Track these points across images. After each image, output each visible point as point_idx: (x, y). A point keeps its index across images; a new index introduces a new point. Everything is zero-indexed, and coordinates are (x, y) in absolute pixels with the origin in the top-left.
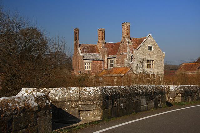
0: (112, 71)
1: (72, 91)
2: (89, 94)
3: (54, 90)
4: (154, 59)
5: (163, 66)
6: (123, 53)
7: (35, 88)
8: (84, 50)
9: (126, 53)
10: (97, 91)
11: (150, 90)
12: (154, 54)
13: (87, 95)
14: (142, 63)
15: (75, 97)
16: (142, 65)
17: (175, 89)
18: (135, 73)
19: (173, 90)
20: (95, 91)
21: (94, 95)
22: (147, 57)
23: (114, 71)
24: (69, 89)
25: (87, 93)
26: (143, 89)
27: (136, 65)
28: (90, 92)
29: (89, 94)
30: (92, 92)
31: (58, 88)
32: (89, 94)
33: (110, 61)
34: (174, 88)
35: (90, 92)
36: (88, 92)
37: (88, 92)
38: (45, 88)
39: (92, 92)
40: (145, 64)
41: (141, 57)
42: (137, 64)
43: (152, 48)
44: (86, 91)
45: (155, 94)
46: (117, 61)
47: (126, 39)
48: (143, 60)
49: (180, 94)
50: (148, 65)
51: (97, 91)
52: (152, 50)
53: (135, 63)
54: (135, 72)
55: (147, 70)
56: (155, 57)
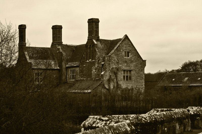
0: (74, 85)
1: (132, 118)
2: (146, 121)
3: (117, 117)
4: (132, 68)
5: (144, 78)
6: (90, 60)
7: (101, 116)
8: (33, 55)
9: (94, 61)
10: (151, 118)
11: (181, 115)
12: (132, 62)
13: (144, 120)
14: (116, 74)
15: (135, 123)
16: (116, 77)
17: (194, 113)
18: (107, 88)
19: (192, 113)
20: (150, 118)
21: (150, 121)
22: (123, 66)
23: (77, 85)
24: (129, 116)
25: (143, 119)
26: (177, 114)
27: (107, 78)
28: (147, 119)
29: (145, 120)
30: (148, 118)
31: (119, 116)
32: (145, 120)
33: (70, 71)
34: (193, 111)
35: (147, 119)
36: (144, 118)
37: (144, 118)
38: (108, 116)
39: (148, 118)
40: (121, 75)
41: (114, 66)
42: (110, 76)
43: (130, 54)
44: (143, 117)
45: (184, 119)
46: (81, 71)
47: (94, 41)
48: (118, 70)
49: (199, 118)
50: (124, 76)
51: (151, 118)
52: (130, 56)
53: (108, 73)
54: (107, 86)
55: (124, 85)
56: (132, 65)
